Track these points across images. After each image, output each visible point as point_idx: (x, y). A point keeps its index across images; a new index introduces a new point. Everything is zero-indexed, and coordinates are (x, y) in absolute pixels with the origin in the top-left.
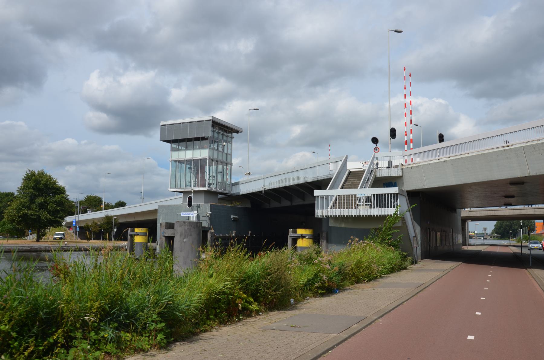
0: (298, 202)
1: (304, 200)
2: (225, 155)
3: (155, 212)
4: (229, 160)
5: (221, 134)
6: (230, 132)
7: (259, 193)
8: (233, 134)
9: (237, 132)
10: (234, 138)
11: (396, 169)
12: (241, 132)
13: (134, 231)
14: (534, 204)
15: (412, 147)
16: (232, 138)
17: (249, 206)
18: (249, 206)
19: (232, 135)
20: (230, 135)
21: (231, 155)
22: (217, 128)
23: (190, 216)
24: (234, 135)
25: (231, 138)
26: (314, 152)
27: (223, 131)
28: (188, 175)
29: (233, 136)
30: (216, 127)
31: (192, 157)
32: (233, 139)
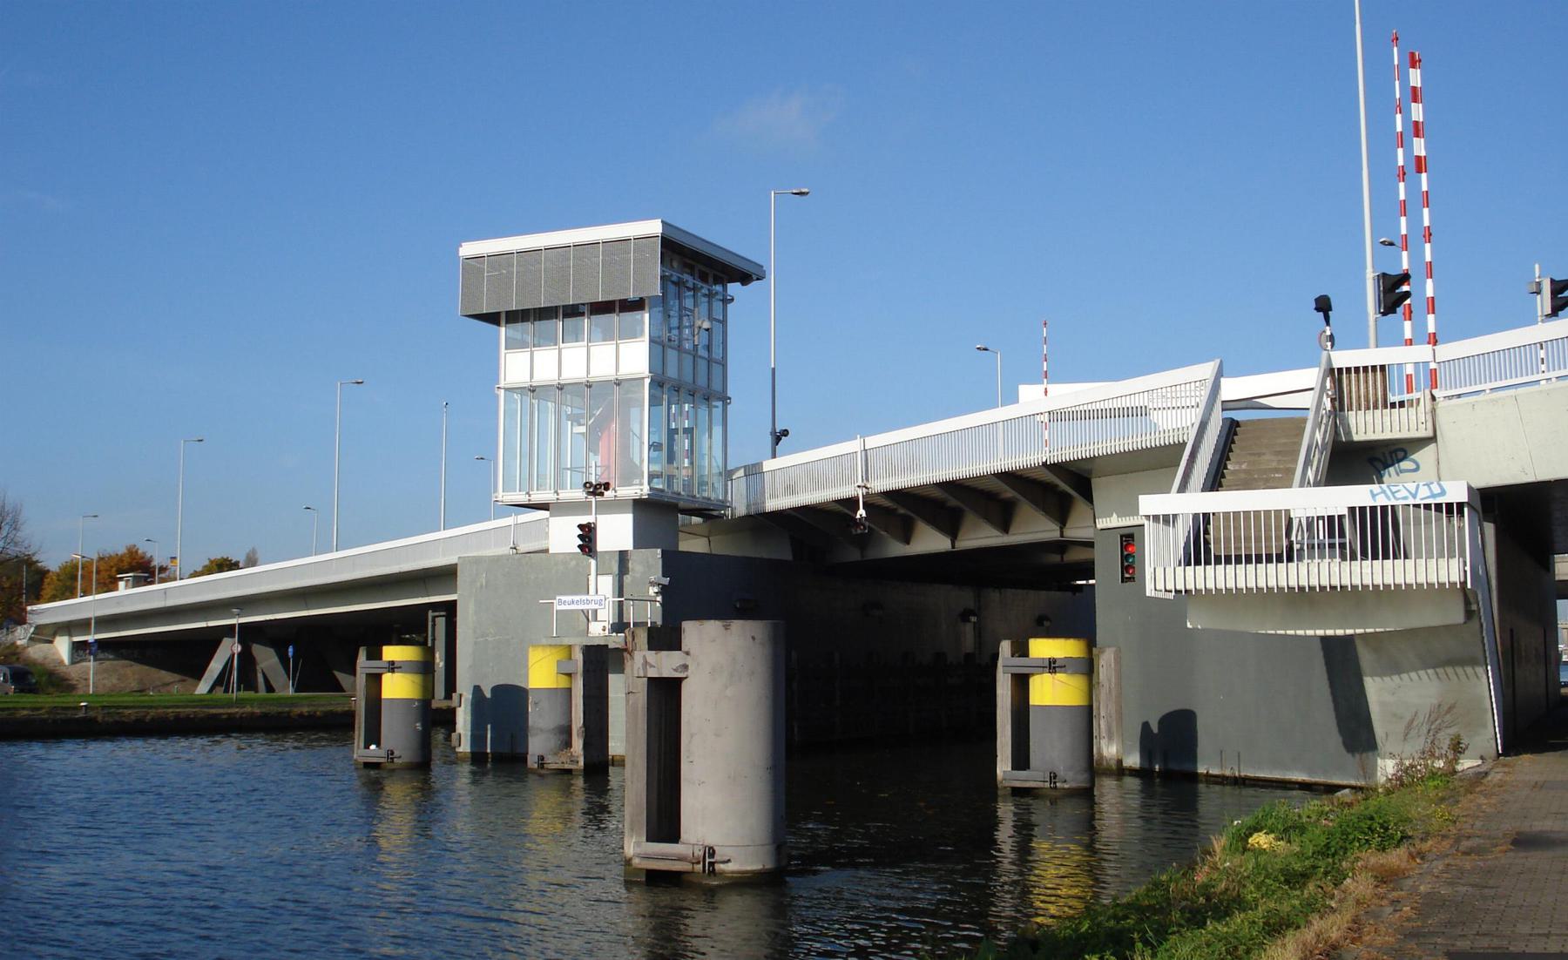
0: (1034, 528)
1: (1005, 528)
2: (702, 365)
3: (445, 576)
4: (716, 385)
5: (673, 282)
6: (718, 281)
7: (794, 513)
8: (730, 285)
9: (745, 278)
10: (732, 300)
11: (1412, 411)
12: (758, 279)
13: (380, 658)
14: (1300, 636)
15: (1408, 335)
16: (726, 301)
17: (785, 554)
18: (785, 554)
19: (725, 289)
20: (718, 288)
21: (723, 365)
22: (675, 264)
23: (1398, 506)
24: (734, 288)
25: (723, 300)
26: (986, 349)
27: (697, 275)
28: (1160, 424)
29: (729, 292)
30: (671, 260)
31: (613, 372)
32: (730, 306)
